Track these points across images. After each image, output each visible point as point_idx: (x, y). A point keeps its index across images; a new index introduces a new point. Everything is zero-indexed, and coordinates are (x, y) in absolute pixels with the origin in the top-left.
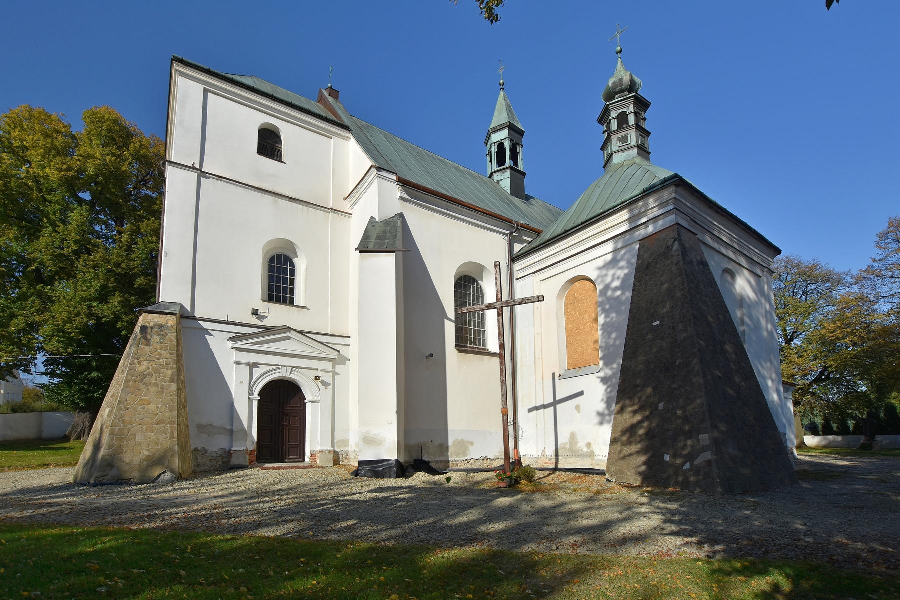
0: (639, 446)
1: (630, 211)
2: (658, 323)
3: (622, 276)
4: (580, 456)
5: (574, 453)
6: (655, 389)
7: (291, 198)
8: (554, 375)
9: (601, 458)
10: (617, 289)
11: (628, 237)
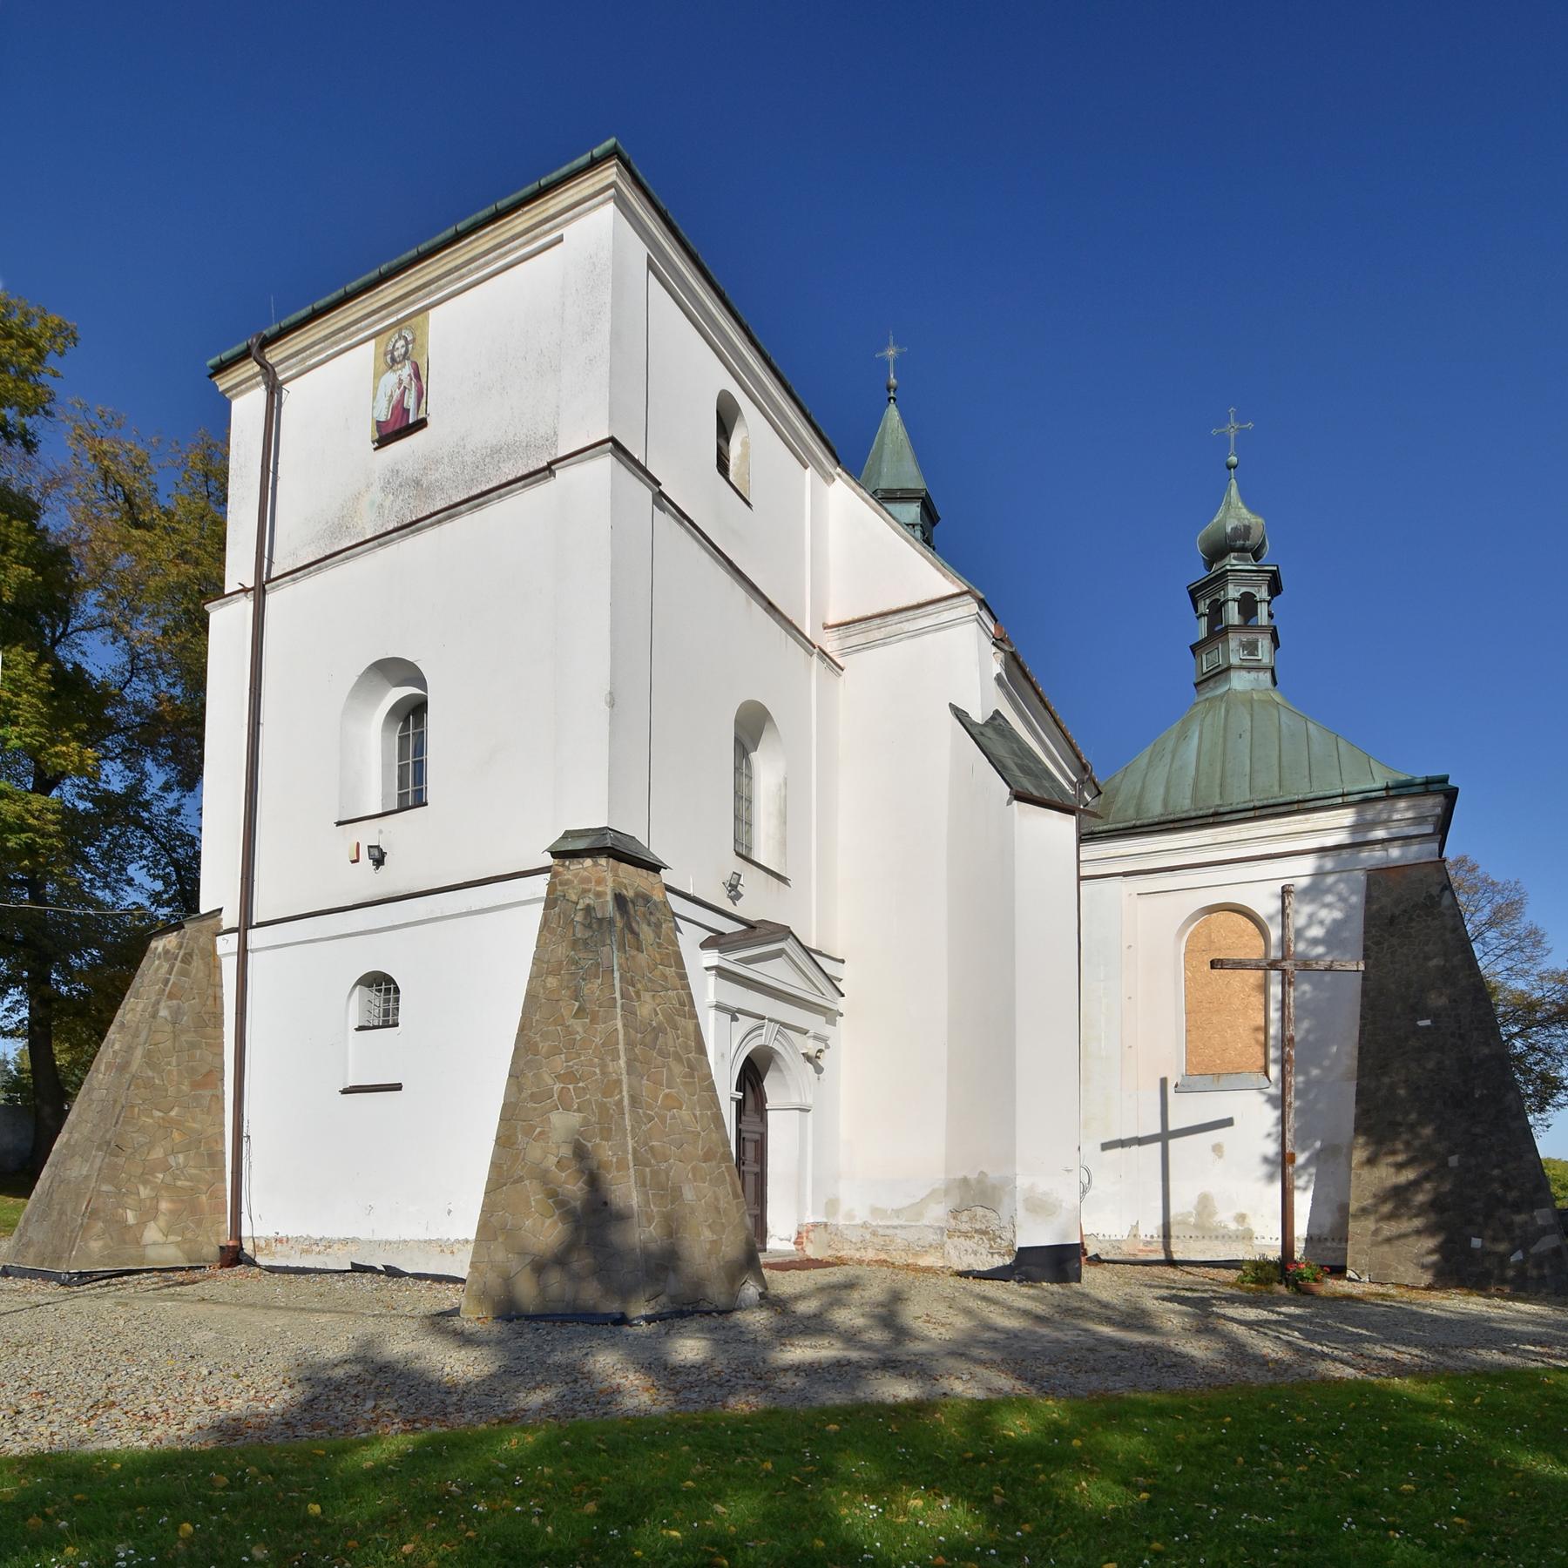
0: (1418, 1223)
1: (1358, 813)
2: (1427, 1022)
3: (1328, 921)
4: (1220, 1238)
5: (1204, 1230)
6: (1439, 1131)
7: (770, 603)
8: (1164, 1082)
9: (1267, 1241)
10: (1315, 942)
11: (1345, 854)
